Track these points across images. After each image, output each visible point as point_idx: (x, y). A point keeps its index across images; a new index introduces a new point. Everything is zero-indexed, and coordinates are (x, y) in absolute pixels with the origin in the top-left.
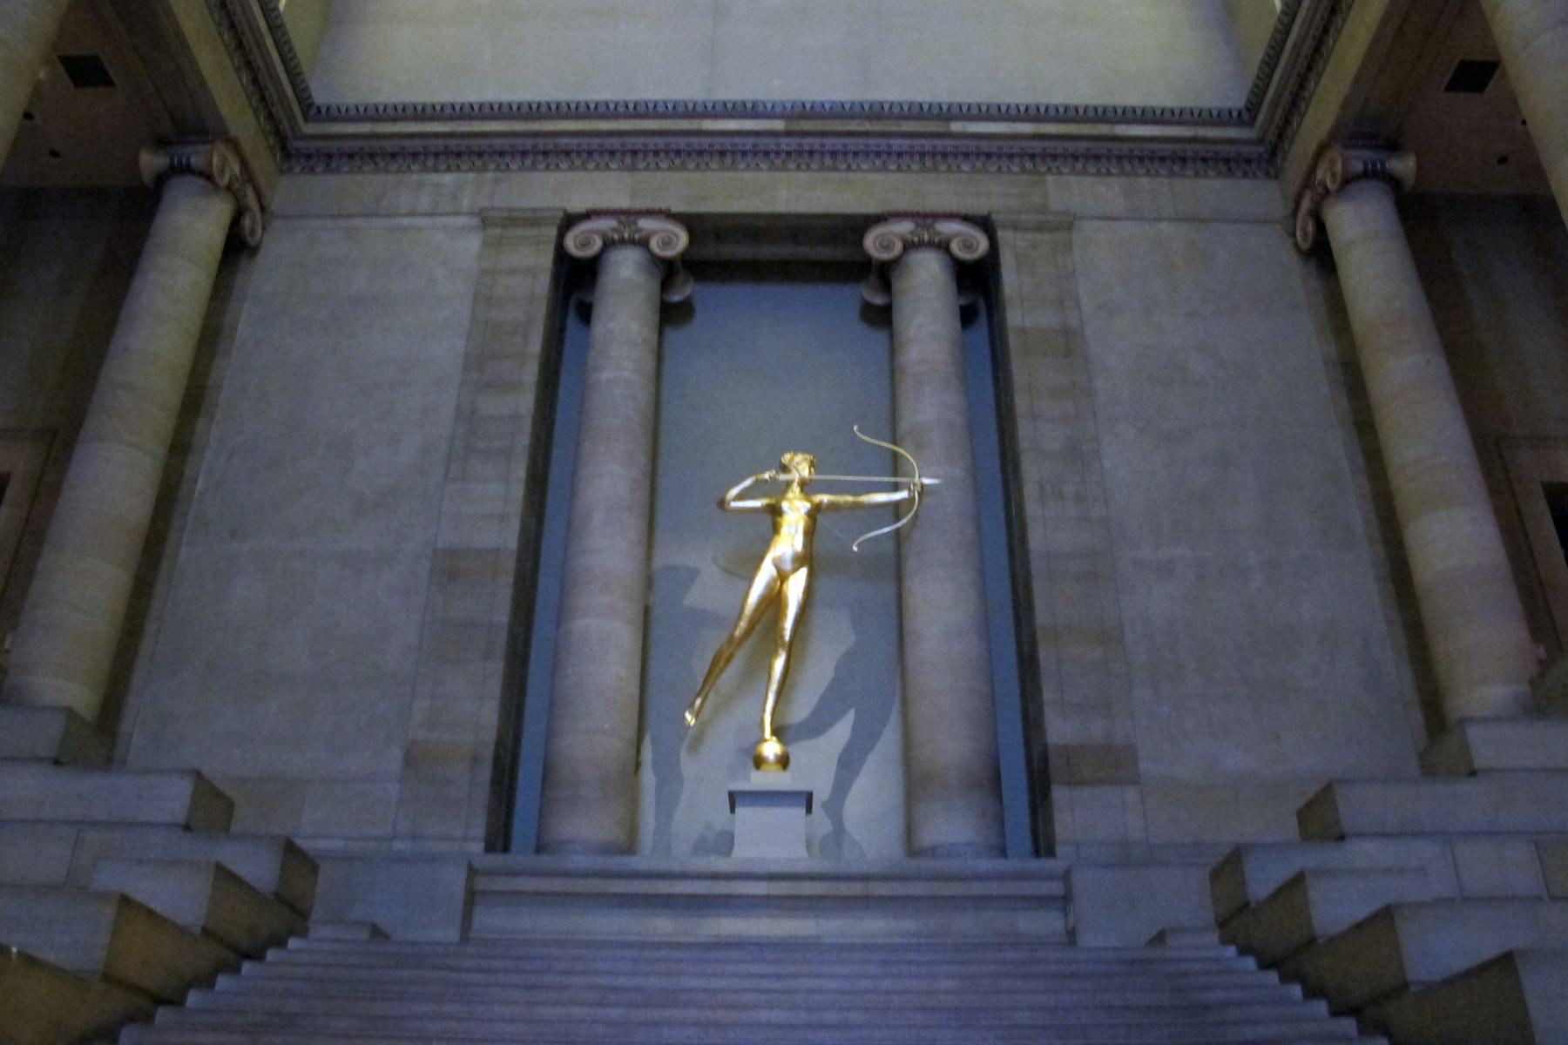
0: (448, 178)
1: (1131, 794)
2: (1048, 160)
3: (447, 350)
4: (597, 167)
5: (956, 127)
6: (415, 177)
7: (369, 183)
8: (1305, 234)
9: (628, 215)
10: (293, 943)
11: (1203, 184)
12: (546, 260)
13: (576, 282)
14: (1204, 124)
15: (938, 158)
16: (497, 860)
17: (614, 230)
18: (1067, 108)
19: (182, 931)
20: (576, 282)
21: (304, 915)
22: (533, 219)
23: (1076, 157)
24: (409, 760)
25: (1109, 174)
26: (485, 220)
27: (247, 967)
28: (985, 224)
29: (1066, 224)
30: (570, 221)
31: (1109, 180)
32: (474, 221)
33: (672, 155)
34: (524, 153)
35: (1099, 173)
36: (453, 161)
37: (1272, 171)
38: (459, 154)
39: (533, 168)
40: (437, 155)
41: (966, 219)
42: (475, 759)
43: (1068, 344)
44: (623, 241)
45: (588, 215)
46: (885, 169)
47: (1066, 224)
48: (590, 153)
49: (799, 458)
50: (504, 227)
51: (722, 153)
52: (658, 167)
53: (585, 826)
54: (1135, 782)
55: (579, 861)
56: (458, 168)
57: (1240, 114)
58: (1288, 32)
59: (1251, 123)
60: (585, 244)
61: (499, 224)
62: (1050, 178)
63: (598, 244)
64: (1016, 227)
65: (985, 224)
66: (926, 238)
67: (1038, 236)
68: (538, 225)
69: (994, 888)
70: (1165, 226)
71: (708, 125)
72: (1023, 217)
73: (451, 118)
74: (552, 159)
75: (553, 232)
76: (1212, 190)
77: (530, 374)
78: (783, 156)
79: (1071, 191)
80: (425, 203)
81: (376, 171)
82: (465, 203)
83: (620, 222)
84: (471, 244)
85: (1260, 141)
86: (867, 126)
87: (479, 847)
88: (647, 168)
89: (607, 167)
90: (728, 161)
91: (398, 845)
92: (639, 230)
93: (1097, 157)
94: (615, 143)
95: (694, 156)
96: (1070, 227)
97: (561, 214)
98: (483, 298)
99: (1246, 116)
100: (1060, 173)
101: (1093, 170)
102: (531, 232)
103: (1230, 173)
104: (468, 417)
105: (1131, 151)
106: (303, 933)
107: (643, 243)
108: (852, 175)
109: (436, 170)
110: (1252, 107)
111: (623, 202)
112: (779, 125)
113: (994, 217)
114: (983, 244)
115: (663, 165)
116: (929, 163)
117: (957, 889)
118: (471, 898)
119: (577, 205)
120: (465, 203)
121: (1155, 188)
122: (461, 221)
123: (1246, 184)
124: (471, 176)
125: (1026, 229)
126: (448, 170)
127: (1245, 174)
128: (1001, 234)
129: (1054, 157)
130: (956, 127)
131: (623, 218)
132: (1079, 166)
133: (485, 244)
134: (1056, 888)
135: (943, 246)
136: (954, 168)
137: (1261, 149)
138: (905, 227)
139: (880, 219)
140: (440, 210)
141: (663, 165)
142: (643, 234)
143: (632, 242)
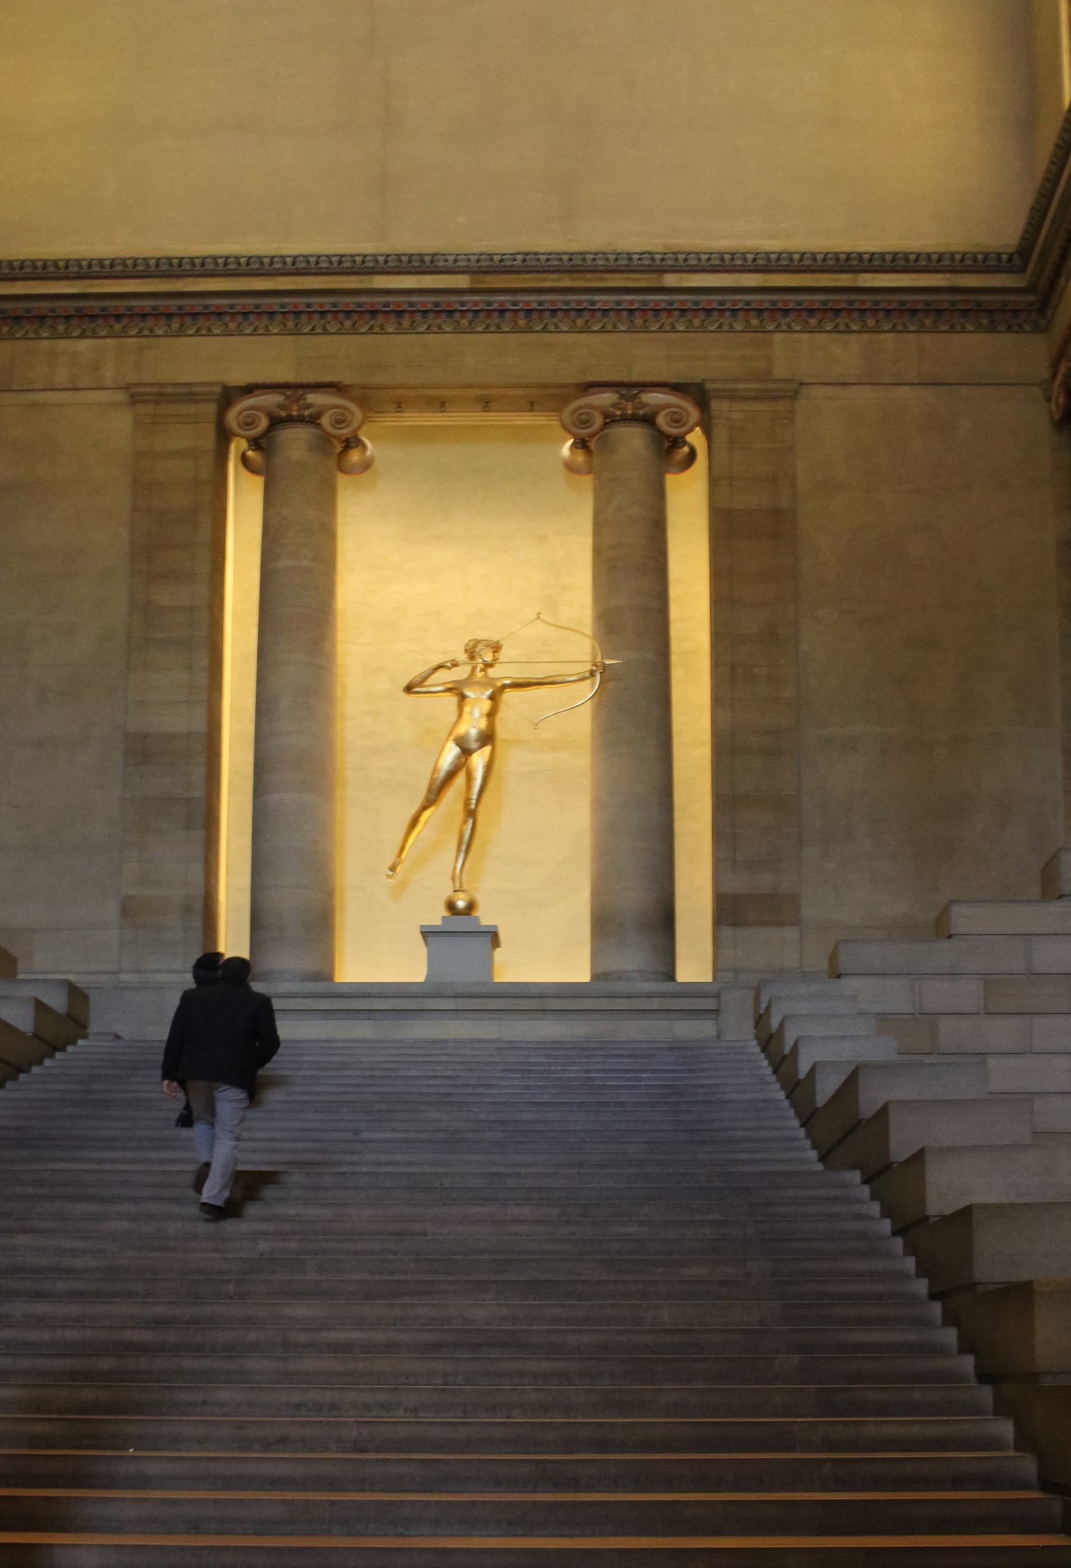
0: (84, 346)
1: (790, 934)
2: (778, 315)
4: (255, 333)
6: (45, 344)
8: (1057, 405)
10: (80, 1042)
11: (957, 339)
14: (968, 271)
15: (650, 314)
17: (280, 406)
19: (23, 1034)
21: (83, 1026)
22: (189, 394)
23: (811, 312)
24: (126, 910)
26: (135, 398)
27: (58, 1055)
29: (791, 391)
30: (228, 396)
31: (846, 337)
33: (341, 316)
34: (169, 316)
35: (836, 330)
37: (1042, 322)
38: (93, 317)
39: (180, 333)
40: (68, 318)
41: (676, 388)
44: (290, 420)
45: (250, 389)
47: (791, 391)
48: (246, 314)
49: (589, 263)
50: (156, 403)
51: (400, 313)
52: (325, 332)
54: (796, 923)
56: (95, 336)
57: (1010, 260)
58: (1056, 184)
59: (1022, 270)
61: (151, 400)
62: (778, 337)
64: (733, 396)
67: (757, 406)
68: (196, 402)
69: (655, 1004)
70: (902, 392)
71: (382, 282)
73: (79, 277)
74: (201, 322)
75: (212, 408)
76: (967, 347)
78: (470, 315)
80: (62, 376)
83: (287, 397)
84: (121, 424)
86: (566, 282)
88: (312, 332)
89: (267, 332)
90: (406, 323)
91: (125, 977)
92: (309, 406)
93: (837, 312)
94: (274, 302)
95: (367, 316)
96: (794, 396)
97: (217, 389)
99: (1017, 262)
100: (790, 331)
103: (992, 328)
106: (85, 1036)
109: (67, 336)
110: (1025, 250)
111: (284, 374)
112: (462, 281)
115: (332, 328)
116: (638, 322)
117: (622, 1004)
119: (238, 377)
121: (900, 348)
122: (105, 396)
123: (1009, 339)
126: (82, 336)
127: (1009, 329)
128: (715, 405)
129: (786, 312)
130: (670, 280)
131: (289, 392)
133: (137, 423)
134: (710, 1004)
135: (648, 420)
137: (1031, 298)
138: (606, 398)
141: (332, 328)
143: (635, 419)
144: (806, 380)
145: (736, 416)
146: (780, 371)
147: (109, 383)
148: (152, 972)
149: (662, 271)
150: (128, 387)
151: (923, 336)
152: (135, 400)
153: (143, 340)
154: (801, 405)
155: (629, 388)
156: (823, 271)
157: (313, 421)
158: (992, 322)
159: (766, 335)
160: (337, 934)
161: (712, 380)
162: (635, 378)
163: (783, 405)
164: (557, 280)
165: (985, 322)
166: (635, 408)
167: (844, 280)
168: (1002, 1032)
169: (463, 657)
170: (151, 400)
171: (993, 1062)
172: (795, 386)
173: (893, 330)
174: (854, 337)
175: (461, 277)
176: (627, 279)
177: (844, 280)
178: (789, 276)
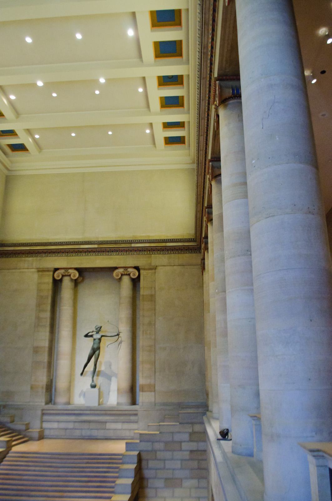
0: (30, 259)
3: (33, 302)
5: (133, 245)
6: (23, 259)
7: (13, 261)
9: (66, 269)
12: (51, 280)
13: (57, 284)
16: (50, 406)
18: (67, 242)
20: (57, 284)
24: (32, 388)
25: (165, 254)
28: (137, 268)
29: (155, 268)
30: (56, 270)
32: (36, 270)
36: (102, 253)
39: (47, 256)
42: (43, 388)
43: (152, 298)
46: (118, 255)
47: (155, 268)
53: (61, 399)
55: (60, 407)
60: (118, 276)
61: (41, 271)
62: (153, 255)
63: (61, 277)
64: (144, 269)
65: (137, 268)
66: (126, 273)
70: (175, 267)
72: (146, 267)
75: (52, 273)
76: (186, 257)
77: (49, 307)
79: (159, 259)
80: (26, 266)
81: (16, 257)
82: (34, 266)
84: (36, 276)
85: (198, 245)
87: (43, 404)
96: (155, 269)
97: (53, 269)
98: (39, 290)
101: (162, 253)
102: (47, 273)
103: (191, 253)
104: (38, 318)
105: (110, 250)
107: (129, 275)
108: (111, 256)
109: (27, 257)
112: (96, 246)
113: (140, 267)
114: (137, 274)
118: (43, 414)
120: (34, 266)
122: (33, 270)
124: (35, 258)
125: (146, 270)
126: (30, 257)
127: (195, 253)
130: (133, 245)
132: (87, 254)
136: (175, 253)
139: (116, 268)
140: (29, 268)
142: (69, 274)
143: (127, 275)
144: (158, 265)
145: (145, 273)
146: (153, 264)
147: (34, 268)
148: (36, 402)
149: (131, 243)
150: (37, 269)
151: (179, 255)
152: (39, 271)
153: (40, 258)
154: (157, 270)
155: (126, 268)
156: (160, 243)
157: (70, 275)
158: (191, 251)
159: (151, 255)
160: (154, 47)
161: (140, 266)
162: (127, 266)
163: (153, 271)
164: (113, 246)
165: (190, 251)
166: (127, 272)
167: (164, 244)
168: (168, 455)
169: (95, 330)
170: (41, 271)
171: (167, 462)
172: (155, 267)
173: (173, 253)
174: (166, 255)
175: (96, 245)
176: (125, 245)
177: (164, 244)
178: (154, 244)
